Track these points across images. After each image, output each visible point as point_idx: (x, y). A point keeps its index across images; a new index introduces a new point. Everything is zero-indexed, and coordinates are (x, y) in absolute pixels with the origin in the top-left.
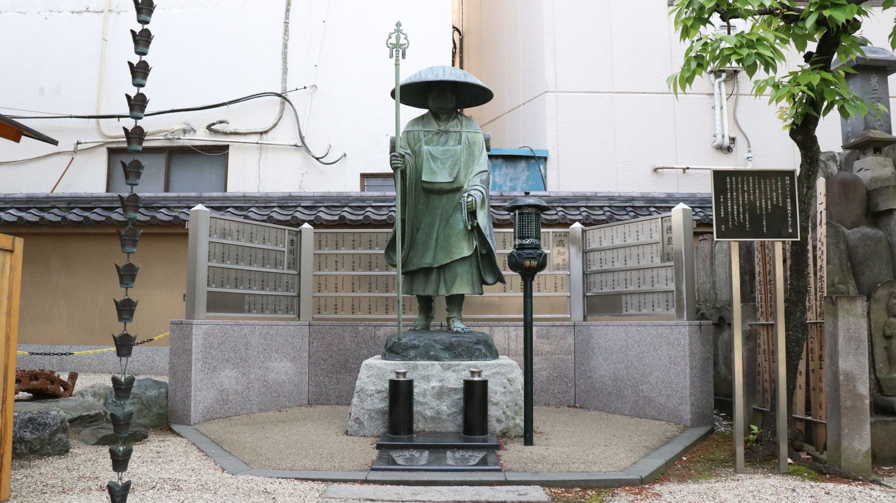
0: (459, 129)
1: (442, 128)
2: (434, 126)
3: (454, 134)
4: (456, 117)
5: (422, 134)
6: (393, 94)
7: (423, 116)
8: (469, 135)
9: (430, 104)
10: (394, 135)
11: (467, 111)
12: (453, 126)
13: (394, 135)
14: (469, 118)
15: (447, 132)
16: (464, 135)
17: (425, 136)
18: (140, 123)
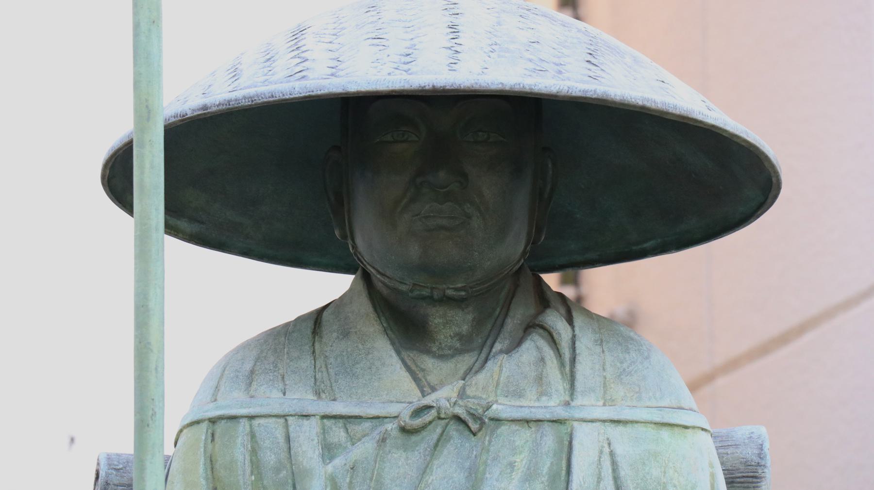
0: (551, 405)
1: (444, 396)
2: (389, 383)
3: (524, 436)
4: (531, 326)
5: (307, 437)
6: (118, 177)
7: (316, 319)
8: (623, 442)
9: (367, 239)
10: (126, 446)
11: (606, 286)
12: (513, 379)
13: (126, 446)
14: (616, 331)
15: (472, 423)
16: (587, 444)
17: (329, 451)
18: (417, 399)
